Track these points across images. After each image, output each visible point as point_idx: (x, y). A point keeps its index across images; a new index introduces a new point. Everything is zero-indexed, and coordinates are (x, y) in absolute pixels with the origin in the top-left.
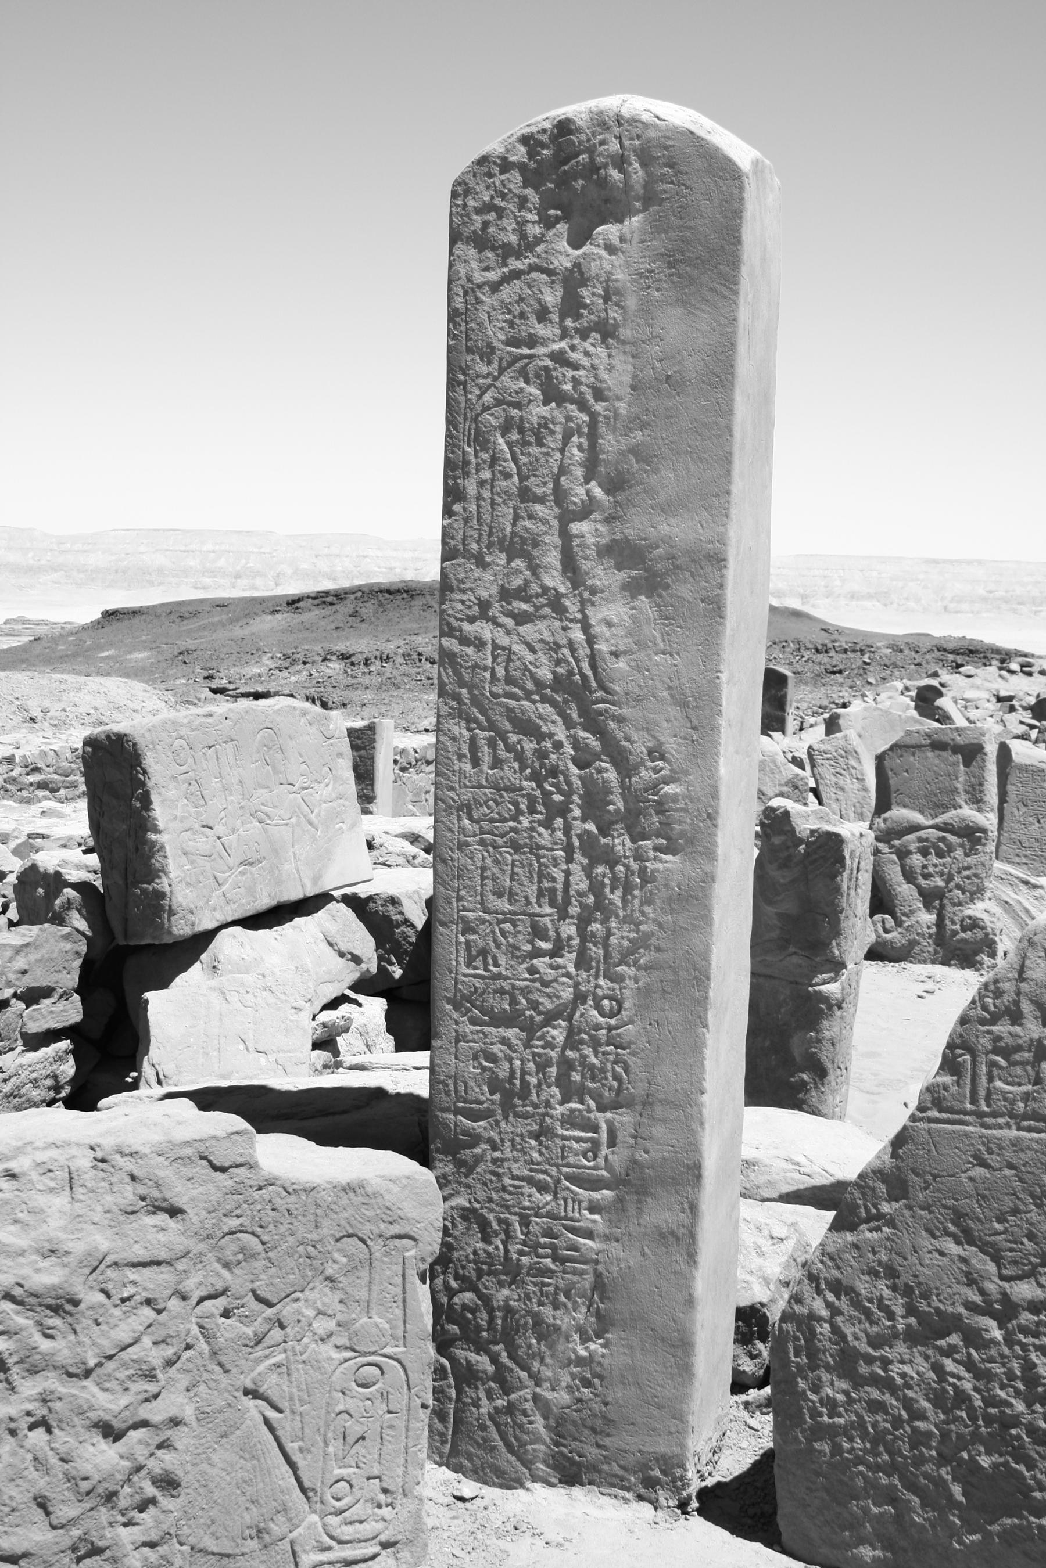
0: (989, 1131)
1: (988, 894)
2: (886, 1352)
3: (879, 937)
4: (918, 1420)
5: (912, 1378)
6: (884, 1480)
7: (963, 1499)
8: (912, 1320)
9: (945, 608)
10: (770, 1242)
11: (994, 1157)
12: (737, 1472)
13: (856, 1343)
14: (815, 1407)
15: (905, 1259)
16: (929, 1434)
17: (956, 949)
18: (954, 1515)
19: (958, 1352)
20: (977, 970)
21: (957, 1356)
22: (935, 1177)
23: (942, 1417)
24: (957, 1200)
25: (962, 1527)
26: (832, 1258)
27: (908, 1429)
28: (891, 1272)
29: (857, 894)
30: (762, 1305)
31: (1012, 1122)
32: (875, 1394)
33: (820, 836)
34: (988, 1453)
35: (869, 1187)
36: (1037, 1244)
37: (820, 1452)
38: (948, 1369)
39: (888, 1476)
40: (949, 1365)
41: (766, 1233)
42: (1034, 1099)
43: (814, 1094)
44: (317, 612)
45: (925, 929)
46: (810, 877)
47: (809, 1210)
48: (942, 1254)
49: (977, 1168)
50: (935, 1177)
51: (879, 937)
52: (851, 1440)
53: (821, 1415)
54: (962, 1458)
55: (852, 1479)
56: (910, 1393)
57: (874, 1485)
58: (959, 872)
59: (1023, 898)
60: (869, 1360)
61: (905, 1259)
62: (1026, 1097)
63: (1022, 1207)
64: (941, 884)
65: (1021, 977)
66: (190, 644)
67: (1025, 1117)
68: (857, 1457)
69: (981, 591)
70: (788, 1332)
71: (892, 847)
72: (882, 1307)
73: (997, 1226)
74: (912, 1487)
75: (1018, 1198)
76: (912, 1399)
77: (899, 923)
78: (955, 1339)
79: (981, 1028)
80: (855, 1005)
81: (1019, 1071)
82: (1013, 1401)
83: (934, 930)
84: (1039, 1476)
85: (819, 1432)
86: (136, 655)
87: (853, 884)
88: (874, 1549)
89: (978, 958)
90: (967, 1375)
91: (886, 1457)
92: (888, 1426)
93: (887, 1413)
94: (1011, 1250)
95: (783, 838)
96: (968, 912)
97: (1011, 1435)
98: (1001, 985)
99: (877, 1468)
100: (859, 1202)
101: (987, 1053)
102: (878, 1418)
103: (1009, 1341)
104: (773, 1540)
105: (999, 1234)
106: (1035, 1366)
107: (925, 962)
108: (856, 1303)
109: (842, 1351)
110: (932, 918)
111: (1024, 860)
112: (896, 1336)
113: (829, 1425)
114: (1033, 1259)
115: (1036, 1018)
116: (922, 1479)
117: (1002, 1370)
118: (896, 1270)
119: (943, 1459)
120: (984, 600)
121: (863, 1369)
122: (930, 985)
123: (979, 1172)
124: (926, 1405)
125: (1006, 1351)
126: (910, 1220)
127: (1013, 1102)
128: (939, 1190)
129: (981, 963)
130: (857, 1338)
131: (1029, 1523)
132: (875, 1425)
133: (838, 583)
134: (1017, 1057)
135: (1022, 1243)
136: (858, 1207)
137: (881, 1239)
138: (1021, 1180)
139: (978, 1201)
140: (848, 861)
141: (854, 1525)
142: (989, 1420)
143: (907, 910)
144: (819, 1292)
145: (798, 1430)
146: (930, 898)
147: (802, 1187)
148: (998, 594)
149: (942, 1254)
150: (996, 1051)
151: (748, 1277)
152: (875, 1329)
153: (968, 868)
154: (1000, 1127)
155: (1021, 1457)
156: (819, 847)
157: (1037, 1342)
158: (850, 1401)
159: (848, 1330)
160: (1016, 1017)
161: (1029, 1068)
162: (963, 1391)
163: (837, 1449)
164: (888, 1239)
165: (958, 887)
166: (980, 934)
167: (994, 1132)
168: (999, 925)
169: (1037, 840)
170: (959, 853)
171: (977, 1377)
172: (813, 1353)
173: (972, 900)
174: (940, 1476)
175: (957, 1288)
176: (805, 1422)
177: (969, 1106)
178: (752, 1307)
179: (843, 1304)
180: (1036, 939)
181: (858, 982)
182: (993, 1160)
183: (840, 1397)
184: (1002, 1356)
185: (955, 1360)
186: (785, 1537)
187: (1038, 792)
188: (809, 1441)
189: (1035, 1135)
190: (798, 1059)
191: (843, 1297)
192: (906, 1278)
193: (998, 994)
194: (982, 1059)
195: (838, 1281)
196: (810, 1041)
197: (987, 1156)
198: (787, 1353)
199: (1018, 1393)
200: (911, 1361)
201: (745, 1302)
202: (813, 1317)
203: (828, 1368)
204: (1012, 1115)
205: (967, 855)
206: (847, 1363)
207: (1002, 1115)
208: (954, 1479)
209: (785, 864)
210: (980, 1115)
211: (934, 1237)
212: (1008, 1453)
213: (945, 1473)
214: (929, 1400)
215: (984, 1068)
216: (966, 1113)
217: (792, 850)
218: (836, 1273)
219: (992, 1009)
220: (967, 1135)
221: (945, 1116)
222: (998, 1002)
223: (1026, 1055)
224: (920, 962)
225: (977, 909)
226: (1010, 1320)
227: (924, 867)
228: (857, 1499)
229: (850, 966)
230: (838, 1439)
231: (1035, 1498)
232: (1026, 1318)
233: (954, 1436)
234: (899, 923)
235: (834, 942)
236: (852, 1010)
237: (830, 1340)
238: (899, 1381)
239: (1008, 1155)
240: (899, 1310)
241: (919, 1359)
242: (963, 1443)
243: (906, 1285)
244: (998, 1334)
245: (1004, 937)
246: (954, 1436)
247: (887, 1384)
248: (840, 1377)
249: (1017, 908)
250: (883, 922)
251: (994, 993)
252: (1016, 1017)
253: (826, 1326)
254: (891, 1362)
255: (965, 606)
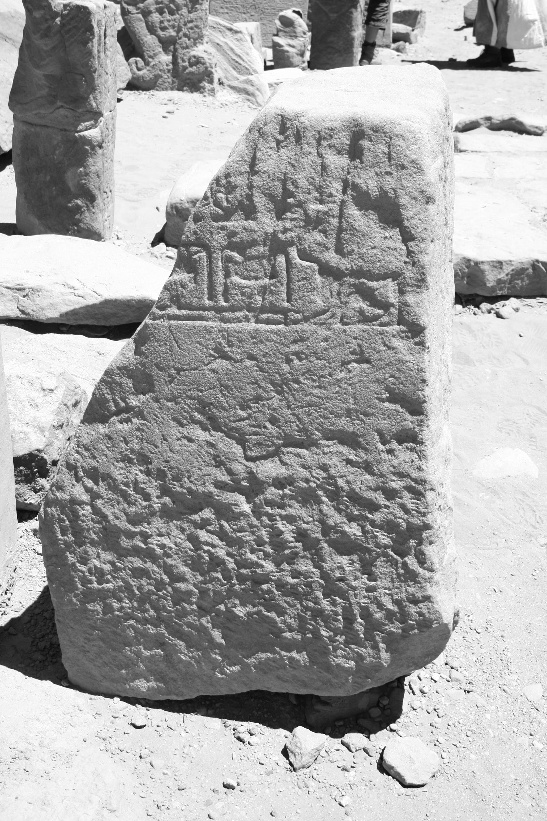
0: (229, 325)
1: (206, 39)
2: (144, 527)
3: (134, 74)
4: (178, 581)
5: (171, 548)
6: (152, 630)
7: (223, 641)
8: (167, 500)
10: (42, 393)
11: (235, 349)
12: (28, 603)
13: (117, 522)
14: (85, 576)
15: (156, 447)
16: (189, 593)
17: (186, 79)
18: (215, 653)
19: (210, 524)
20: (202, 93)
21: (209, 528)
22: (179, 371)
23: (200, 578)
24: (201, 391)
25: (223, 661)
26: (87, 449)
27: (170, 589)
28: (144, 459)
29: (106, 56)
30: (39, 451)
31: (250, 315)
32: (138, 563)
33: (71, 9)
34: (243, 604)
35: (116, 383)
36: (279, 427)
37: (93, 611)
38: (203, 539)
39: (156, 627)
40: (203, 535)
41: (38, 386)
42: (271, 292)
43: (87, 214)
45: (165, 67)
46: (67, 44)
47: (80, 339)
48: (190, 440)
49: (219, 360)
50: (179, 371)
51: (134, 74)
52: (120, 600)
53: (91, 582)
54: (220, 610)
55: (124, 631)
56: (169, 561)
57: (145, 634)
58: (185, 25)
59: (228, 40)
60: (130, 535)
61: (156, 447)
62: (264, 291)
63: (264, 395)
64: (174, 34)
65: (253, 170)
67: (263, 310)
68: (127, 614)
70: (53, 515)
71: (138, 9)
72: (137, 489)
73: (241, 413)
74: (178, 634)
75: (260, 387)
76: (172, 566)
77: (147, 64)
78: (207, 513)
79: (215, 224)
80: (113, 143)
81: (254, 265)
82: (263, 562)
83: (171, 67)
84: (288, 620)
85: (90, 596)
87: (102, 49)
88: (148, 681)
89: (201, 85)
90: (220, 543)
91: (152, 613)
92: (152, 588)
93: (150, 578)
94: (256, 434)
95: (42, 12)
96: (193, 53)
97: (262, 590)
98: (232, 179)
99: (146, 621)
100: (108, 396)
101: (222, 249)
102: (143, 582)
103: (257, 512)
104: (61, 678)
105: (243, 420)
106: (282, 533)
107: (166, 89)
108: (113, 487)
109: (104, 528)
110: (169, 58)
111: (226, 11)
112: (153, 514)
113: (99, 590)
114: (276, 441)
115: (269, 211)
116: (186, 629)
117: (252, 537)
118: (148, 457)
119: (203, 611)
121: (125, 543)
122: (171, 107)
123: (220, 364)
124: (185, 569)
125: (255, 521)
126: (157, 412)
127: (251, 296)
128: (183, 383)
129: (204, 88)
130: (117, 518)
131: (282, 657)
132: (140, 588)
134: (252, 251)
135: (265, 427)
136: (108, 401)
137: (131, 429)
138: (262, 370)
139: (221, 391)
140: (96, 29)
141: (129, 664)
142: (242, 579)
143: (151, 54)
144: (78, 479)
145: (72, 595)
146: (167, 44)
147: (77, 307)
149: (190, 440)
150: (231, 246)
151: (25, 429)
152: (133, 509)
153: (191, 21)
154: (240, 321)
155: (271, 606)
156: (72, 19)
157: (283, 512)
158: (116, 569)
159: (108, 511)
160: (250, 212)
161: (265, 262)
162: (218, 557)
163: (108, 609)
164: (138, 429)
165: (185, 35)
166: (202, 68)
167: (234, 325)
168: (214, 61)
170: (184, 11)
171: (229, 544)
172: (78, 532)
173: (195, 44)
174: (201, 624)
175: (206, 470)
176: (77, 589)
177: (207, 302)
178: (31, 454)
179: (102, 488)
180: (266, 129)
181: (113, 125)
182: (234, 352)
183: (107, 567)
184: (251, 526)
185: (208, 531)
186: (70, 675)
188: (83, 603)
189: (274, 327)
190: (72, 189)
191: (101, 483)
192: (157, 464)
193: (230, 188)
194: (218, 255)
195: (95, 469)
196: (80, 175)
197: (227, 349)
198: (54, 533)
199: (267, 556)
200: (168, 534)
201: (22, 451)
202: (74, 501)
203: (93, 543)
204: (250, 309)
205: (190, 12)
206: (110, 538)
207: (240, 309)
208: (213, 627)
209: (46, 34)
210: (219, 310)
211: (182, 425)
212: (260, 604)
213: (206, 621)
214: (187, 565)
215: (220, 264)
216: (205, 309)
217: (50, 22)
218: (93, 462)
219: (225, 204)
220: (207, 330)
221: (184, 312)
222: (230, 197)
223: (262, 249)
224: (163, 89)
225: (199, 51)
226: (257, 495)
227: (161, 22)
228: (130, 645)
229: (106, 114)
230: (108, 601)
231: (286, 638)
232: (272, 492)
233: (211, 593)
234: (147, 64)
235: (91, 97)
236: (111, 147)
237: (93, 520)
238: (159, 551)
239: (248, 347)
240: (154, 492)
241: (176, 532)
242: (220, 598)
243: (159, 470)
244: (246, 508)
245: (218, 69)
246: (211, 593)
247: (149, 555)
248: (104, 550)
249: (225, 48)
250: (136, 63)
251: (226, 188)
252: (250, 212)
253: (88, 508)
254: (150, 536)
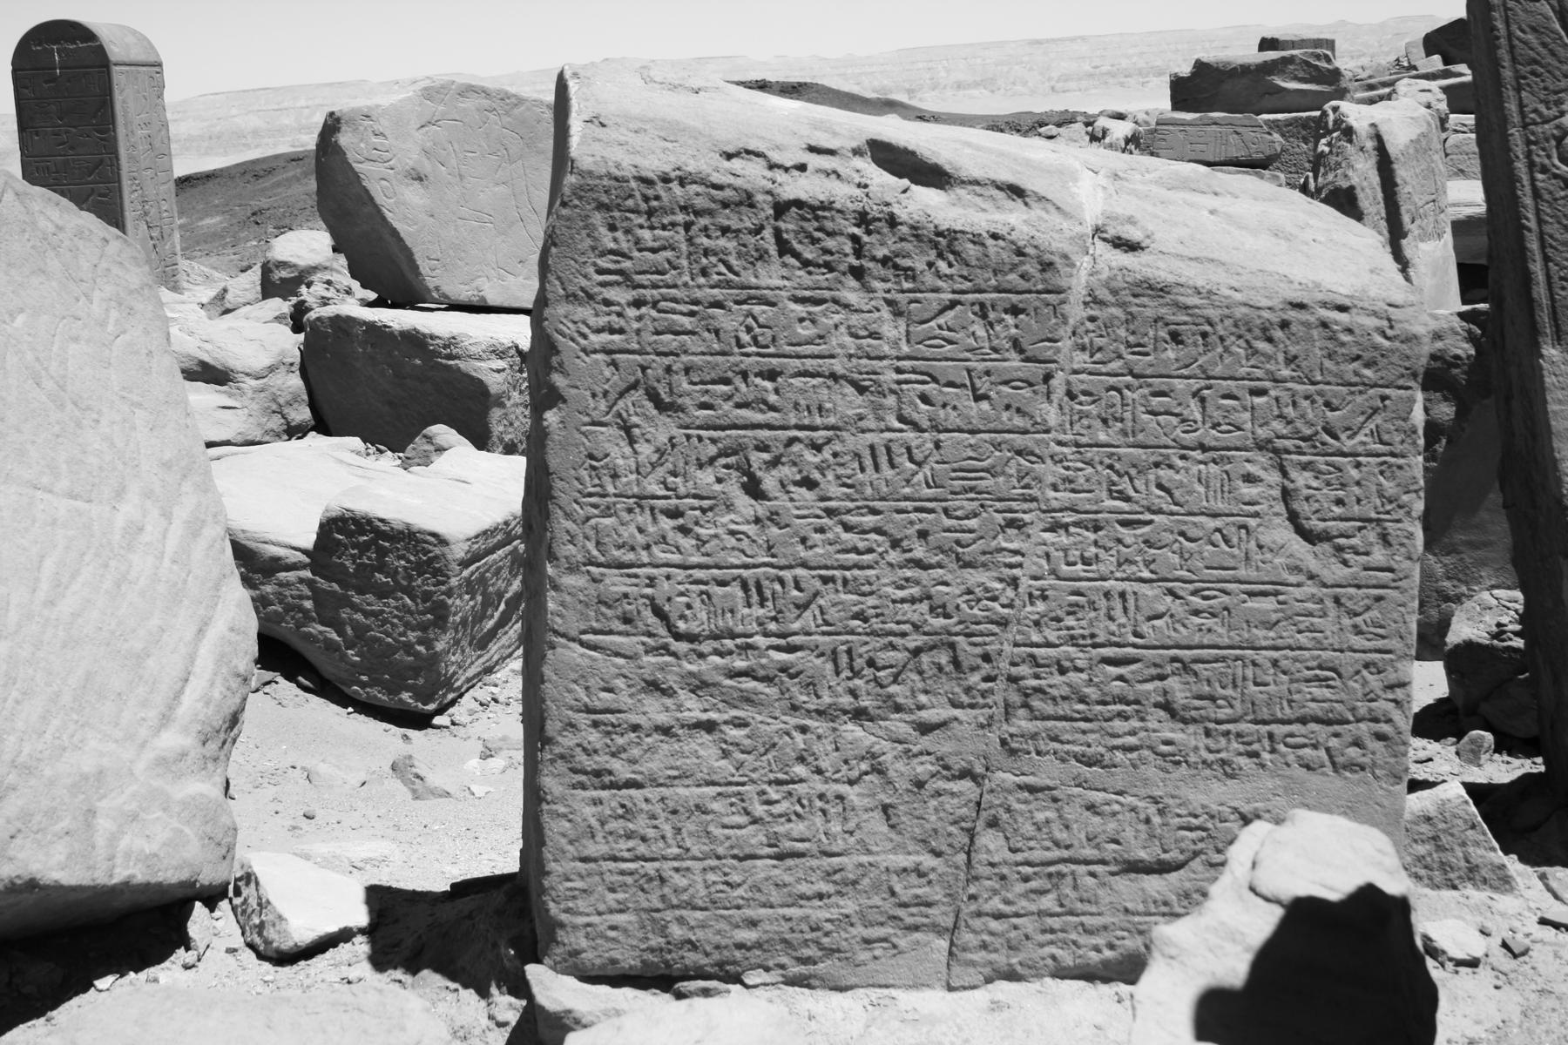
9: (1053, 88)
66: (264, 202)
69: (1087, 68)
86: (208, 221)
111: (694, 709)
120: (1091, 76)
133: (943, 74)
148: (1104, 69)
169: (755, 591)
187: (728, 321)
255: (1072, 85)
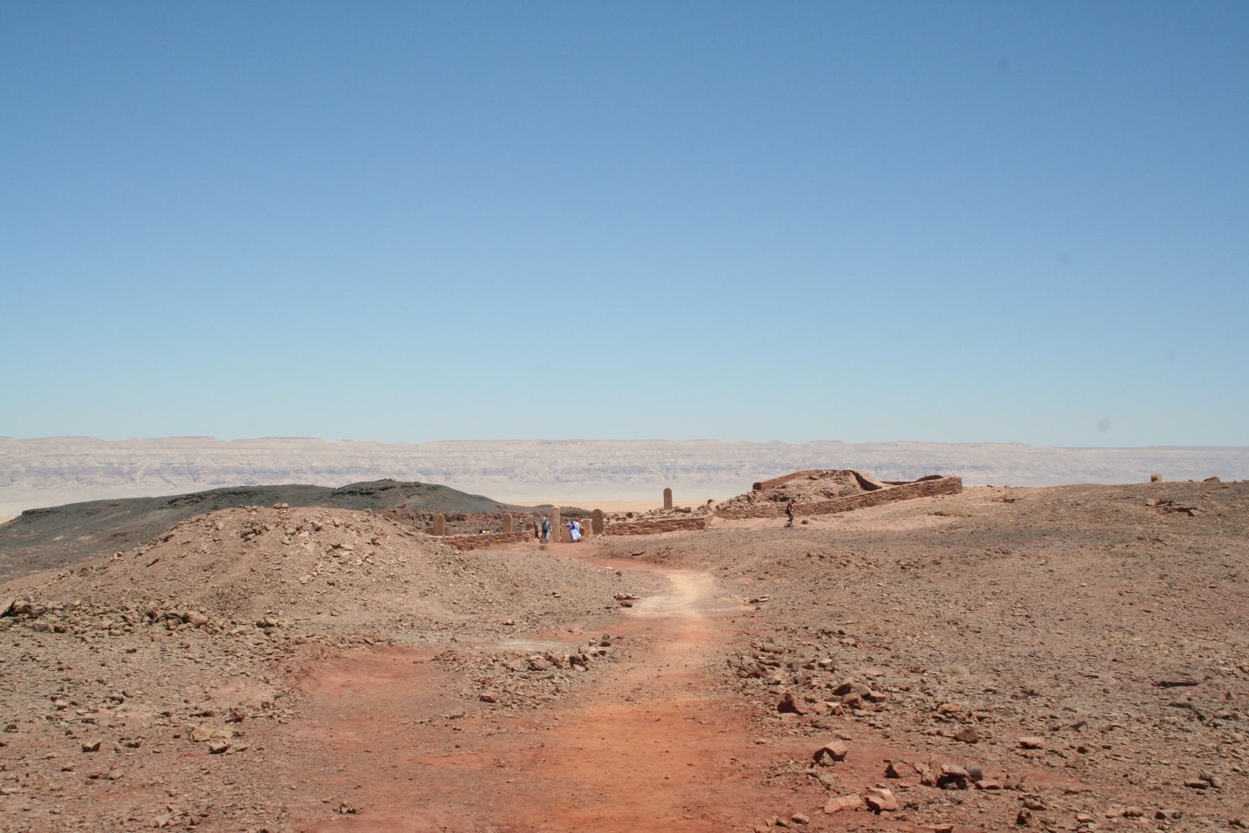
44: (188, 507)
69: (584, 464)
133: (473, 462)
220: (748, 535)
255: (573, 477)
